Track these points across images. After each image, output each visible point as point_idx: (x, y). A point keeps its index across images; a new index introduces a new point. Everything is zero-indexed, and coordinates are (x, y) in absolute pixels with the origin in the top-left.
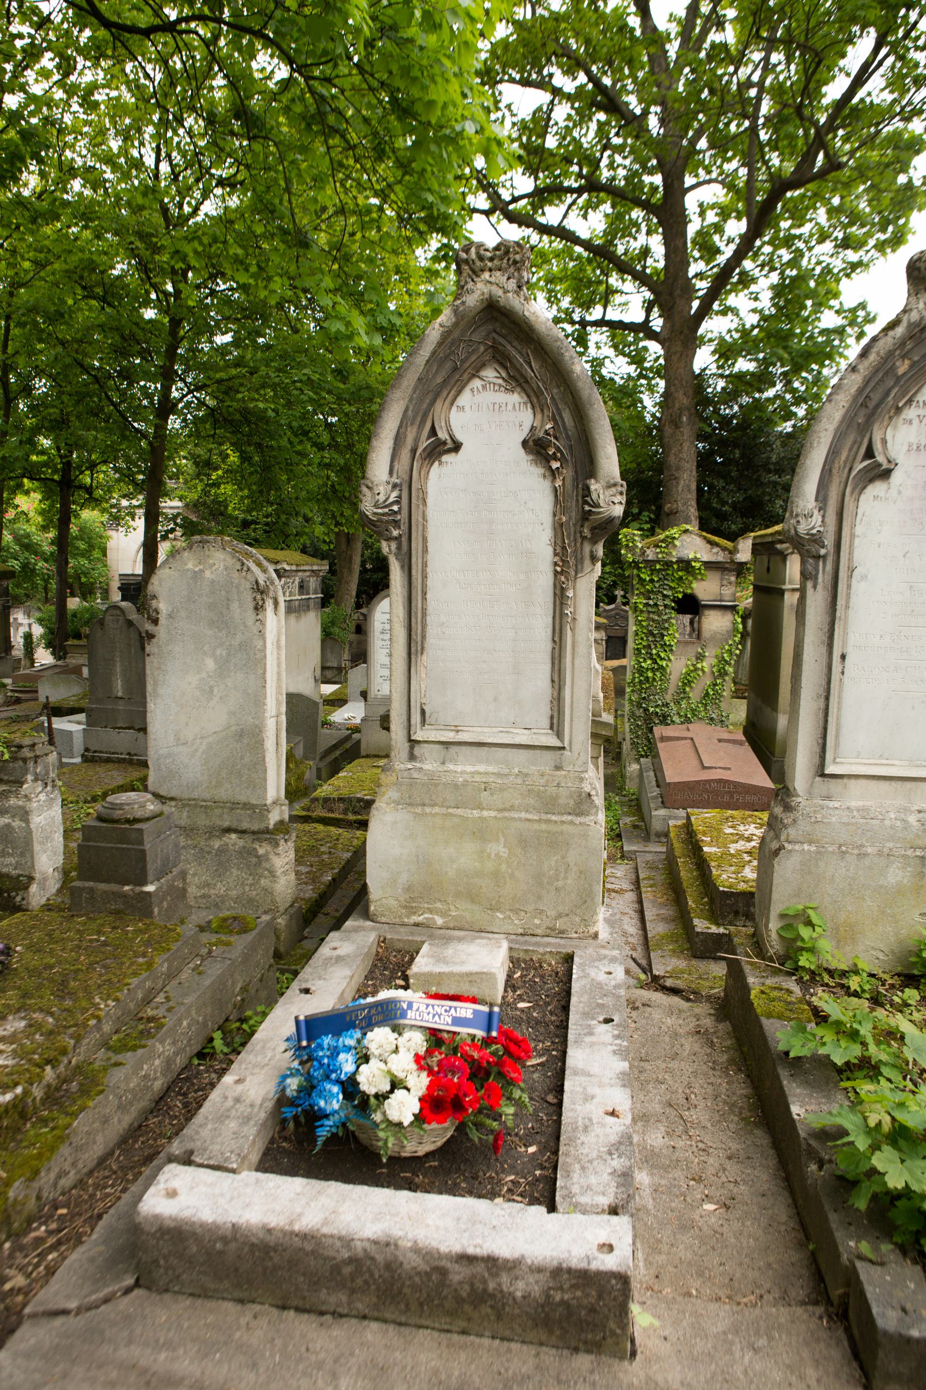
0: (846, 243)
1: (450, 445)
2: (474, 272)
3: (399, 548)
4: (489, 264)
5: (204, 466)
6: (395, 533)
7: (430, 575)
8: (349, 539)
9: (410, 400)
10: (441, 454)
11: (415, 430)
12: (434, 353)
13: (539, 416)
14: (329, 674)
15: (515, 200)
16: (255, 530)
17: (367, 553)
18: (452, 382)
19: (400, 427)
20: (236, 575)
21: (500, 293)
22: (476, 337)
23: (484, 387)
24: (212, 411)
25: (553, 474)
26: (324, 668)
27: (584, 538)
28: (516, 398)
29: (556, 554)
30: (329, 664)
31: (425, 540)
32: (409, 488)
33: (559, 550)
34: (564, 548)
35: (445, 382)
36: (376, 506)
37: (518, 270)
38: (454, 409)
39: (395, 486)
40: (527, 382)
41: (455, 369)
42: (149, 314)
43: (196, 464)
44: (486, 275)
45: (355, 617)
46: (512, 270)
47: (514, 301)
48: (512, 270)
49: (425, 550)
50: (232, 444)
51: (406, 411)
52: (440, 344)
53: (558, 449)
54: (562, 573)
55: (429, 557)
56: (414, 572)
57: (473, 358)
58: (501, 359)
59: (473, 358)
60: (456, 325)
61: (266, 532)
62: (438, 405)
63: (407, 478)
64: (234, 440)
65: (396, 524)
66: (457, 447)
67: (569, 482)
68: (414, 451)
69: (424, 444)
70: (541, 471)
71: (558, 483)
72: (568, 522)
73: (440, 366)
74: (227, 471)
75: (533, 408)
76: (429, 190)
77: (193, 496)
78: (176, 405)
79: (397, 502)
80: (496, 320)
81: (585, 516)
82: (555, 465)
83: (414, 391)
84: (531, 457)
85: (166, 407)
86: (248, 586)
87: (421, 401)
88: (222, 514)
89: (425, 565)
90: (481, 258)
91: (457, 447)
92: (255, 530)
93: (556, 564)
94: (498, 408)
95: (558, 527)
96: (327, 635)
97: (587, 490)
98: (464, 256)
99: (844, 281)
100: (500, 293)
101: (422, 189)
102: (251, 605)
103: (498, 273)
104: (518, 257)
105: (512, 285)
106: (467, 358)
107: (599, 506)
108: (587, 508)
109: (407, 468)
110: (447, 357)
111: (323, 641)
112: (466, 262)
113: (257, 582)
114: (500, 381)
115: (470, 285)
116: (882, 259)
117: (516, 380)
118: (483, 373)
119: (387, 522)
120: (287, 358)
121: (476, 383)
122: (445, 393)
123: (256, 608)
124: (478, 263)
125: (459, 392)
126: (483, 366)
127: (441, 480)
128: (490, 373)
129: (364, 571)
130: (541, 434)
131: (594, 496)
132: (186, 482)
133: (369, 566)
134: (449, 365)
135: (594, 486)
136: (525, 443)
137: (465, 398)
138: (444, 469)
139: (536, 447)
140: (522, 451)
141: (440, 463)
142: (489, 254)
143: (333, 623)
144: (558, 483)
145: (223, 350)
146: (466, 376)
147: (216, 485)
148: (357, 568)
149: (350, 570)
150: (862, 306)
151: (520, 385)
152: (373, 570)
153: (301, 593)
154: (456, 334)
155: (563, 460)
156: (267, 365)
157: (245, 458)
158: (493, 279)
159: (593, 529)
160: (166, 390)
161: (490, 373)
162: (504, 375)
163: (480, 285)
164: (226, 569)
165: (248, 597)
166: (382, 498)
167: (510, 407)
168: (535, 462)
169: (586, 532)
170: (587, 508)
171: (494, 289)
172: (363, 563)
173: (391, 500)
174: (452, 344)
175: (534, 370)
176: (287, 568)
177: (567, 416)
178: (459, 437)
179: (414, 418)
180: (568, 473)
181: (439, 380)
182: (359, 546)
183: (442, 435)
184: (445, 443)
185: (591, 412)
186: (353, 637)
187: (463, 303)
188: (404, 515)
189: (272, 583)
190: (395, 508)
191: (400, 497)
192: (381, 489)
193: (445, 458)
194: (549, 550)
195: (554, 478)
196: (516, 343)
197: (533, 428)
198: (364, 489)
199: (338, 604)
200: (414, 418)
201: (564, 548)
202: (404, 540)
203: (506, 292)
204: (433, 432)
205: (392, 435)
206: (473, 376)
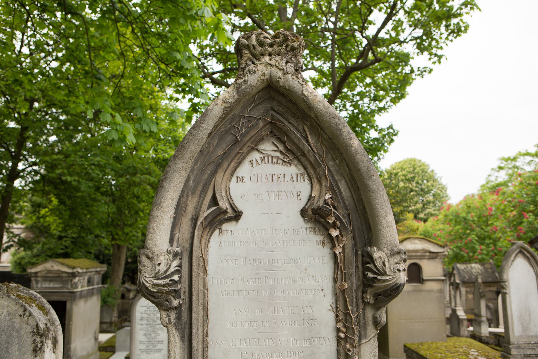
0: (376, 98)
1: (230, 213)
2: (254, 56)
3: (179, 317)
4: (270, 49)
5: (36, 206)
6: (175, 303)
7: (210, 345)
8: (119, 247)
9: (192, 171)
10: (221, 222)
11: (196, 199)
12: (216, 127)
13: (316, 186)
14: (105, 326)
15: (214, 73)
16: (65, 241)
17: (129, 253)
18: (233, 153)
19: (181, 196)
20: (19, 319)
21: (280, 74)
22: (256, 114)
23: (263, 159)
24: (43, 176)
25: (332, 242)
26: (101, 323)
27: (366, 304)
28: (293, 170)
29: (338, 321)
30: (105, 320)
31: (206, 309)
32: (190, 258)
33: (341, 317)
34: (347, 314)
35: (226, 154)
36: (157, 276)
37: (295, 55)
38: (234, 179)
39: (176, 255)
40: (304, 155)
41: (236, 142)
42: (12, 125)
43: (33, 206)
44: (267, 59)
45: (121, 289)
46: (290, 55)
47: (293, 82)
48: (290, 55)
49: (206, 319)
50: (55, 195)
51: (187, 181)
52: (222, 118)
53: (338, 218)
54: (346, 339)
55: (210, 325)
56: (194, 343)
57: (253, 133)
58: (278, 133)
59: (253, 133)
60: (238, 101)
61: (72, 242)
62: (219, 176)
63: (187, 246)
64: (56, 193)
65: (177, 294)
66: (237, 216)
67: (349, 250)
68: (195, 220)
69: (205, 212)
70: (320, 238)
71: (338, 250)
72: (350, 288)
73: (222, 138)
74: (51, 210)
75: (310, 179)
76: (178, 51)
77: (30, 222)
78: (19, 173)
79: (178, 272)
80: (274, 99)
81: (367, 284)
82: (335, 233)
83: (196, 163)
84: (309, 225)
85: (14, 174)
86: (29, 329)
87: (202, 171)
88: (47, 233)
89: (205, 334)
90: (261, 44)
91: (237, 216)
92: (65, 241)
93: (338, 330)
94: (277, 178)
95: (340, 295)
96: (105, 304)
97: (369, 258)
98: (245, 42)
99: (377, 116)
100: (280, 74)
101: (174, 50)
102: (30, 348)
103: (278, 58)
104: (295, 44)
105: (290, 68)
106: (247, 133)
107: (385, 274)
108: (370, 275)
109: (187, 236)
110: (227, 131)
111: (102, 307)
112: (247, 47)
113: (37, 326)
114: (278, 154)
115: (251, 67)
116: (394, 105)
117: (293, 153)
118: (261, 147)
119: (168, 293)
120: (86, 148)
121: (255, 156)
122: (226, 165)
123: (35, 351)
124: (259, 48)
125: (239, 164)
126: (262, 140)
127: (222, 250)
128: (268, 147)
129: (127, 263)
130: (321, 204)
131: (379, 264)
132: (26, 215)
133: (129, 260)
134: (229, 139)
135: (377, 254)
136: (303, 212)
137: (245, 170)
138: (225, 237)
139: (315, 216)
140: (301, 219)
141: (221, 231)
142: (269, 41)
143: (108, 295)
144: (338, 250)
145: (52, 145)
146: (245, 149)
147: (44, 217)
148: (123, 263)
149: (119, 264)
150: (391, 127)
151: (297, 158)
152: (131, 263)
153: (88, 285)
154: (237, 111)
155: (342, 228)
156: (76, 154)
157: (61, 202)
158: (273, 62)
159: (376, 296)
160: (15, 165)
161: (268, 147)
162: (281, 148)
163: (260, 67)
164: (9, 314)
165: (28, 341)
166: (162, 268)
167: (288, 178)
168: (313, 230)
169: (369, 298)
170: (370, 275)
171: (274, 70)
172: (127, 259)
173: (172, 269)
174: (233, 119)
175: (312, 144)
176: (80, 271)
177: (343, 186)
178: (240, 206)
179: (195, 188)
180: (347, 240)
181: (220, 152)
182: (124, 250)
183: (223, 204)
184: (225, 212)
185: (370, 183)
186: (119, 301)
187: (245, 82)
188: (183, 287)
189: (53, 324)
190: (176, 278)
191: (180, 266)
192: (162, 259)
193: (225, 226)
194: (331, 316)
195: (333, 246)
196: (292, 120)
197: (310, 197)
198: (144, 259)
199: (112, 284)
200: (195, 188)
201: (347, 314)
202: (185, 309)
203: (285, 73)
204: (214, 201)
205: (174, 204)
206: (253, 149)
